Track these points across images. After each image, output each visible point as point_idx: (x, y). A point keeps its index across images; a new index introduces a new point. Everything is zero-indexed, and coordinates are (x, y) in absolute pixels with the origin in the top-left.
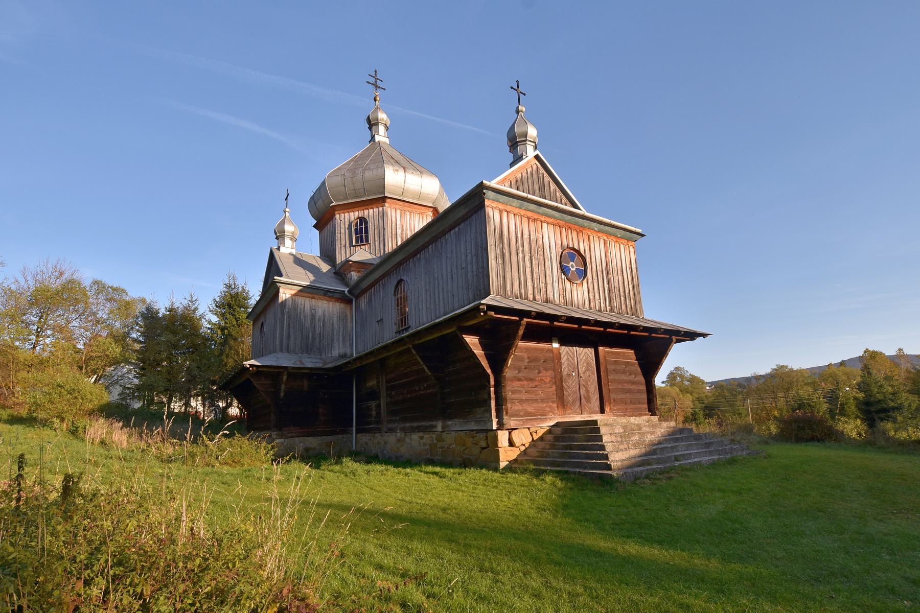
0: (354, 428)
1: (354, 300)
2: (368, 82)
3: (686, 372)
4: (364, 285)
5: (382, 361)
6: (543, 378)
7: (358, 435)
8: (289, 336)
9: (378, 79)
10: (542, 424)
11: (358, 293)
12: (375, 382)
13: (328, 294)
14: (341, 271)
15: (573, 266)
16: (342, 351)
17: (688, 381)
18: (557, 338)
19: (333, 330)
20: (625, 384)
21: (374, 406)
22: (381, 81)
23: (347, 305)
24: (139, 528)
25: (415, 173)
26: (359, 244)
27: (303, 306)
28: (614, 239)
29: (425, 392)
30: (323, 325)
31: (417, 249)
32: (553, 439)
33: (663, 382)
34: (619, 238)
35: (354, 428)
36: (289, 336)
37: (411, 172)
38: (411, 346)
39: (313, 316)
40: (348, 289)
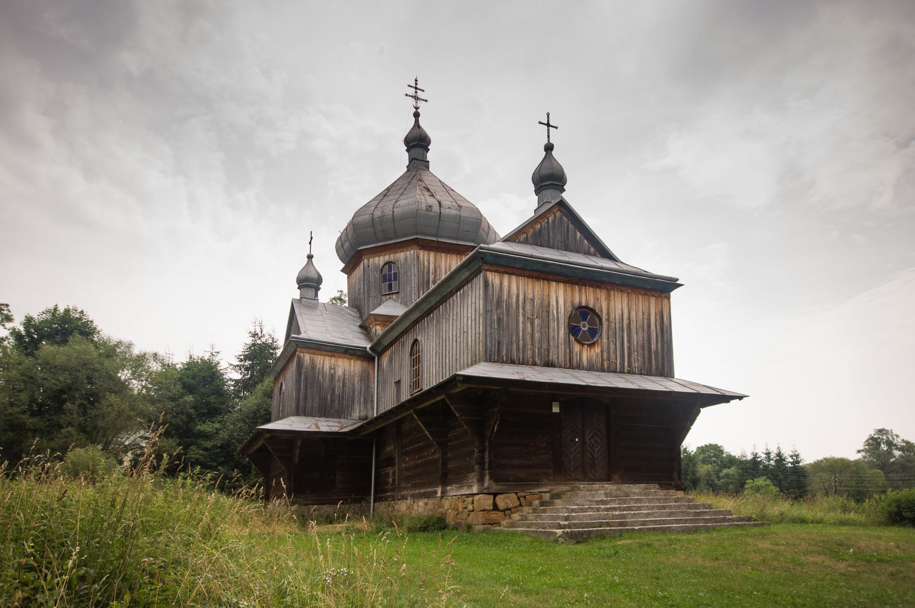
0: (372, 496)
1: (376, 358)
3: (895, 437)
4: (386, 342)
5: (399, 423)
8: (306, 398)
10: (533, 489)
12: (393, 447)
14: (366, 324)
15: (585, 327)
16: (363, 414)
17: (899, 449)
19: (354, 391)
21: (391, 472)
22: (423, 91)
23: (370, 363)
27: (322, 365)
28: (642, 292)
29: (432, 457)
30: (343, 385)
31: (431, 308)
32: (539, 504)
33: (859, 451)
34: (649, 289)
35: (372, 496)
36: (306, 398)
38: (413, 411)
39: (332, 376)
40: (370, 345)
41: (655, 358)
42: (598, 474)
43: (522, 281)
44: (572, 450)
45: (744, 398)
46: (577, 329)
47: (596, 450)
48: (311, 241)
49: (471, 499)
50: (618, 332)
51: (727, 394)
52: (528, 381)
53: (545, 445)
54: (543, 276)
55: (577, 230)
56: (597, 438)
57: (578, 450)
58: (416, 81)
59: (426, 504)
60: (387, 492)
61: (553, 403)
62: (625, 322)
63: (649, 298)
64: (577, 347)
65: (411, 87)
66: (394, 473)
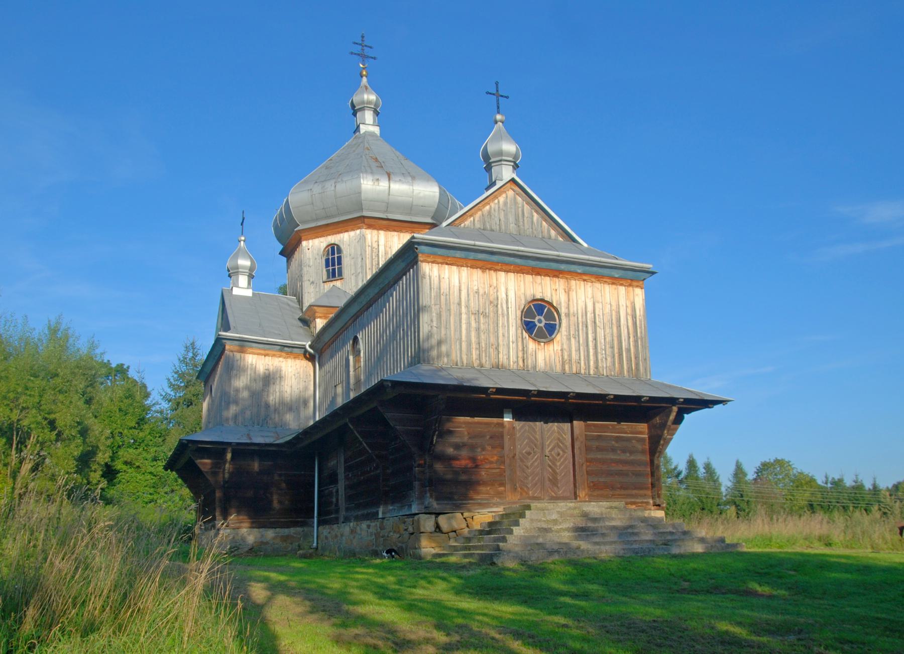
2: (352, 53)
6: (487, 457)
7: (321, 528)
9: (366, 46)
11: (321, 347)
13: (286, 349)
15: (540, 322)
18: (511, 410)
20: (613, 465)
22: (371, 47)
24: (21, 377)
25: (404, 180)
26: (331, 279)
37: (398, 179)
38: (348, 420)
40: (310, 343)
41: (627, 357)
42: (561, 492)
43: (465, 271)
44: (529, 464)
45: (729, 403)
46: (531, 325)
47: (558, 464)
48: (243, 222)
49: (411, 519)
50: (580, 327)
51: (706, 398)
52: (466, 386)
53: (495, 458)
54: (489, 266)
55: (533, 211)
56: (559, 450)
57: (536, 464)
58: (363, 37)
59: (369, 527)
60: (332, 513)
61: (504, 410)
62: (590, 316)
63: (618, 288)
64: (531, 345)
65: (357, 44)
66: (337, 491)
